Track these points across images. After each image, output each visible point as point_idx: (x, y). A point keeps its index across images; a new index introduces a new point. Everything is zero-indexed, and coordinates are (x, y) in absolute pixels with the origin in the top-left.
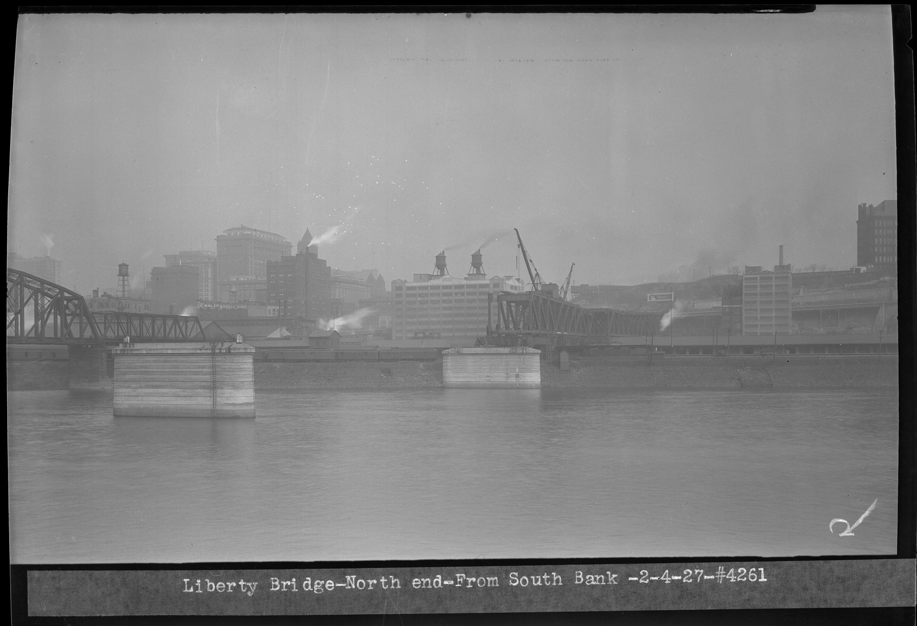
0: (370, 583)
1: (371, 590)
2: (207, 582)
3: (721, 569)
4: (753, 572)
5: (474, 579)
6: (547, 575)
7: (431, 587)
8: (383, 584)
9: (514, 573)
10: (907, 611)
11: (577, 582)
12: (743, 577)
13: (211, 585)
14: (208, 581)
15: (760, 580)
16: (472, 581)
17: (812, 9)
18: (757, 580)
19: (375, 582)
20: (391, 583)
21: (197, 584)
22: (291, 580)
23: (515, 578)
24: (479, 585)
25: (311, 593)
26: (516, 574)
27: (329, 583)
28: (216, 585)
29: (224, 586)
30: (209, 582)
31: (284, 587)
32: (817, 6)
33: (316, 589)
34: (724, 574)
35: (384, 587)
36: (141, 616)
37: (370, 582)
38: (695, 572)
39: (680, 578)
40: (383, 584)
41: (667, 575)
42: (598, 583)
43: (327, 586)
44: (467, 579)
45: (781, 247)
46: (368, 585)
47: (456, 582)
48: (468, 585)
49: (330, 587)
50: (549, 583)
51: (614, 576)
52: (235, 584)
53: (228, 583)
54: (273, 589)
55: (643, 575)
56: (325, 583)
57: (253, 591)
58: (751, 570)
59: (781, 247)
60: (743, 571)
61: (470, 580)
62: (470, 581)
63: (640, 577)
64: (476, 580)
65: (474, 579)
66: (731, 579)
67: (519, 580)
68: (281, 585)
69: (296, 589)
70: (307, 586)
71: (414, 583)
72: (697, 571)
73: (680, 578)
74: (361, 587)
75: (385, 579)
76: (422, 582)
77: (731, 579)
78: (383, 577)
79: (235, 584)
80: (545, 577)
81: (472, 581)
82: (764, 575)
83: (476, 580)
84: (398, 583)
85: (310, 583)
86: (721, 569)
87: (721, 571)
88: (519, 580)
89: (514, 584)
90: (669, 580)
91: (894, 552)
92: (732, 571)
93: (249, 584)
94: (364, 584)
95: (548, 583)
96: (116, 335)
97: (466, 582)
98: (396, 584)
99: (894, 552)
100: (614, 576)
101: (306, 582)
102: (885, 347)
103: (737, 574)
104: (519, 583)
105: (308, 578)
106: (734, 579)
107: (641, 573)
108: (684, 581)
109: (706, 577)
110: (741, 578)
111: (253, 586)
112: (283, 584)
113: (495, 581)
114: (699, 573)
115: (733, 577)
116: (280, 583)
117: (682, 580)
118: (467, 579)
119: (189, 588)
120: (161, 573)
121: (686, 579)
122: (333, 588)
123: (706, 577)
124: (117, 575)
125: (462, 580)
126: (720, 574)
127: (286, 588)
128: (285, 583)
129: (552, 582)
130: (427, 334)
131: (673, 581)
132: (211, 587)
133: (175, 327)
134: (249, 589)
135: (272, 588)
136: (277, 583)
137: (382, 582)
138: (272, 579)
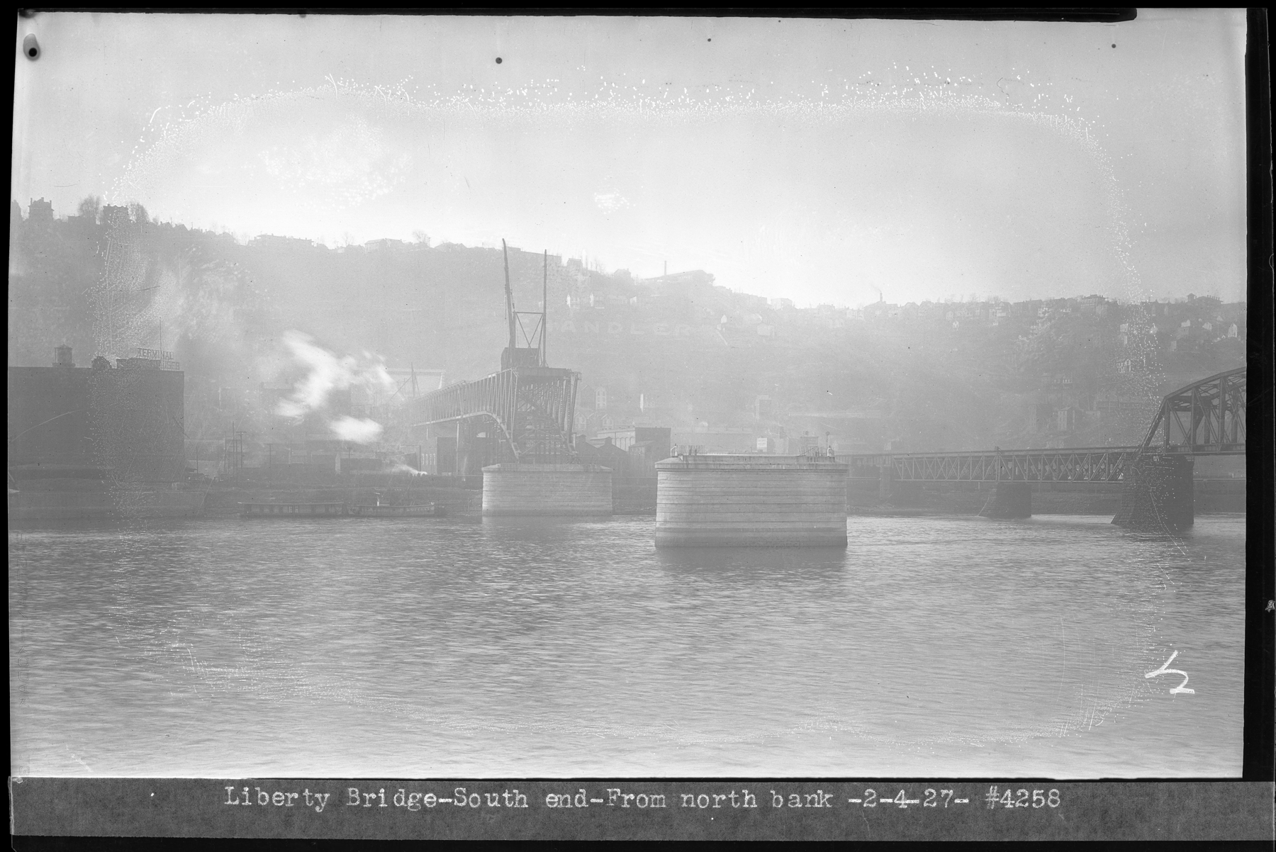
1: (249, 806)
2: (744, 794)
5: (632, 796)
7: (695, 806)
8: (307, 798)
9: (461, 789)
10: (1267, 844)
11: (350, 804)
12: (1024, 802)
13: (777, 799)
14: (774, 793)
17: (1131, 16)
19: (724, 797)
20: (744, 801)
21: (243, 793)
23: (638, 798)
24: (701, 806)
25: (404, 809)
26: (464, 790)
27: (429, 798)
29: (283, 798)
30: (776, 794)
32: (1139, 10)
33: (410, 804)
34: (997, 797)
35: (308, 804)
36: (599, 841)
37: (717, 798)
39: (859, 801)
42: (658, 806)
46: (712, 801)
47: (606, 800)
48: (380, 804)
50: (739, 804)
51: (827, 796)
52: (296, 796)
53: (288, 794)
54: (230, 802)
55: (929, 797)
56: (424, 796)
57: (323, 805)
60: (1023, 795)
61: (626, 797)
62: (717, 800)
63: (863, 798)
64: (636, 798)
65: (632, 796)
67: (468, 799)
68: (363, 800)
69: (385, 803)
70: (399, 800)
71: (548, 800)
73: (859, 801)
74: (703, 805)
76: (286, 797)
77: (900, 804)
80: (506, 795)
81: (370, 798)
83: (636, 798)
84: (525, 801)
88: (468, 799)
90: (905, 804)
91: (1240, 775)
92: (1008, 792)
93: (318, 796)
94: (708, 800)
97: (621, 799)
98: (521, 801)
99: (1240, 775)
100: (827, 796)
103: (1014, 797)
104: (468, 803)
105: (581, 790)
106: (1011, 804)
108: (865, 805)
109: (957, 801)
110: (869, 802)
111: (323, 798)
112: (807, 797)
113: (662, 799)
116: (361, 796)
117: (861, 804)
119: (233, 800)
121: (1020, 802)
122: (435, 804)
123: (957, 801)
125: (615, 797)
126: (992, 797)
128: (717, 798)
131: (880, 804)
132: (263, 798)
134: (317, 803)
135: (227, 801)
136: (357, 796)
137: (305, 796)
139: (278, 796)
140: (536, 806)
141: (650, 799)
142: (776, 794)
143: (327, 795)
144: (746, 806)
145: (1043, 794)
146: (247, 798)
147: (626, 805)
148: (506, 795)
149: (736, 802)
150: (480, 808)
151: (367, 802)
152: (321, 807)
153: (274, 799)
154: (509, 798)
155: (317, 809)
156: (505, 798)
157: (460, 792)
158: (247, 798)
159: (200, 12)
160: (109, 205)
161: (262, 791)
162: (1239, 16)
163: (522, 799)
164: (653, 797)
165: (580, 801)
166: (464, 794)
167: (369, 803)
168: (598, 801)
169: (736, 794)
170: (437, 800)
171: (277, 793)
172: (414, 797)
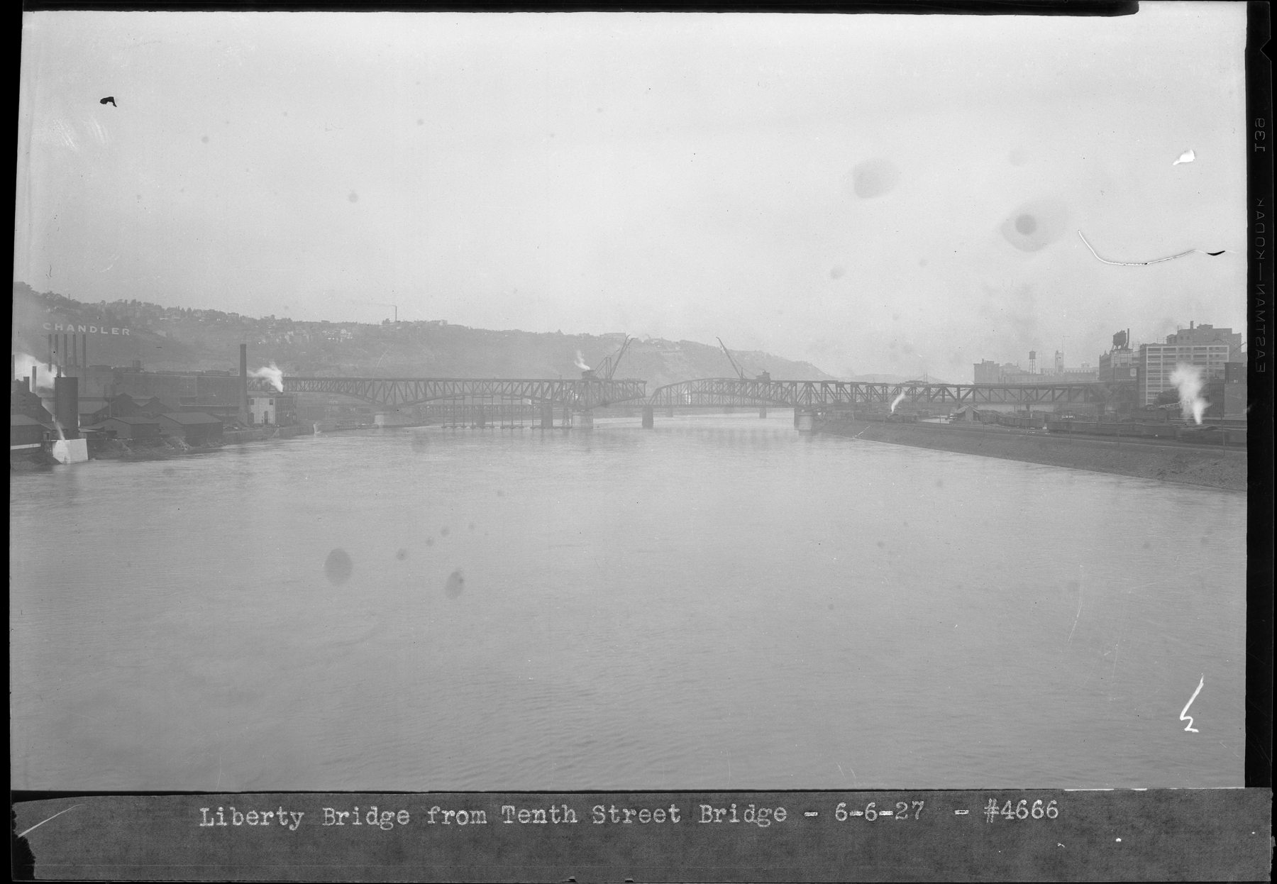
0: (265, 817)
3: (992, 803)
4: (1037, 806)
5: (452, 813)
6: (283, 811)
8: (553, 815)
11: (326, 824)
15: (218, 824)
16: (344, 816)
18: (712, 821)
19: (347, 814)
20: (564, 815)
21: (218, 813)
22: (351, 810)
27: (659, 813)
28: (245, 817)
29: (664, 815)
31: (718, 815)
37: (265, 815)
38: (912, 804)
40: (553, 815)
41: (1010, 807)
43: (399, 818)
44: (443, 812)
45: (243, 347)
48: (732, 818)
49: (403, 820)
55: (902, 809)
56: (638, 813)
57: (298, 823)
58: (1035, 803)
59: (243, 347)
61: (447, 814)
62: (341, 816)
66: (1007, 815)
67: (1030, 811)
68: (261, 819)
69: (224, 821)
70: (372, 818)
72: (915, 803)
75: (615, 808)
77: (1007, 815)
78: (673, 805)
79: (272, 816)
81: (268, 816)
82: (203, 815)
85: (753, 812)
86: (992, 803)
87: (992, 806)
89: (1024, 817)
91: (86, 457)
95: (615, 819)
96: (471, 389)
98: (570, 817)
101: (748, 811)
102: (1243, 422)
107: (898, 805)
112: (263, 816)
114: (917, 806)
115: (1009, 813)
118: (443, 812)
119: (209, 821)
120: (166, 797)
124: (143, 802)
127: (343, 822)
129: (563, 818)
130: (577, 420)
132: (238, 819)
133: (395, 390)
138: (326, 809)
139: (403, 814)
140: (419, 819)
141: (470, 815)
142: (568, 809)
143: (301, 814)
144: (566, 821)
145: (1026, 806)
146: (222, 819)
147: (446, 822)
148: (612, 811)
149: (556, 818)
150: (605, 825)
151: (265, 821)
152: (295, 825)
153: (248, 818)
154: (284, 815)
155: (291, 827)
156: (671, 813)
157: (599, 810)
158: (222, 819)
159: (490, 12)
160: (983, 360)
161: (237, 811)
162: (35, 24)
163: (541, 814)
164: (473, 813)
165: (372, 818)
166: (603, 812)
167: (224, 821)
168: (812, 814)
169: (615, 808)
170: (773, 813)
171: (523, 810)
172: (386, 816)
